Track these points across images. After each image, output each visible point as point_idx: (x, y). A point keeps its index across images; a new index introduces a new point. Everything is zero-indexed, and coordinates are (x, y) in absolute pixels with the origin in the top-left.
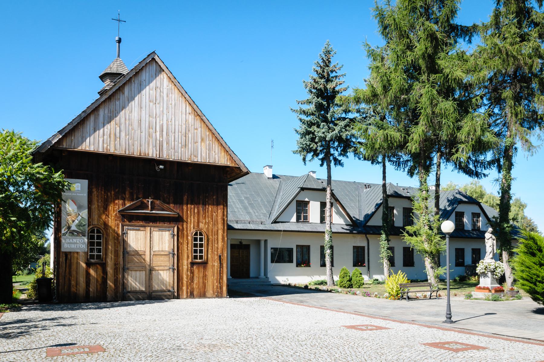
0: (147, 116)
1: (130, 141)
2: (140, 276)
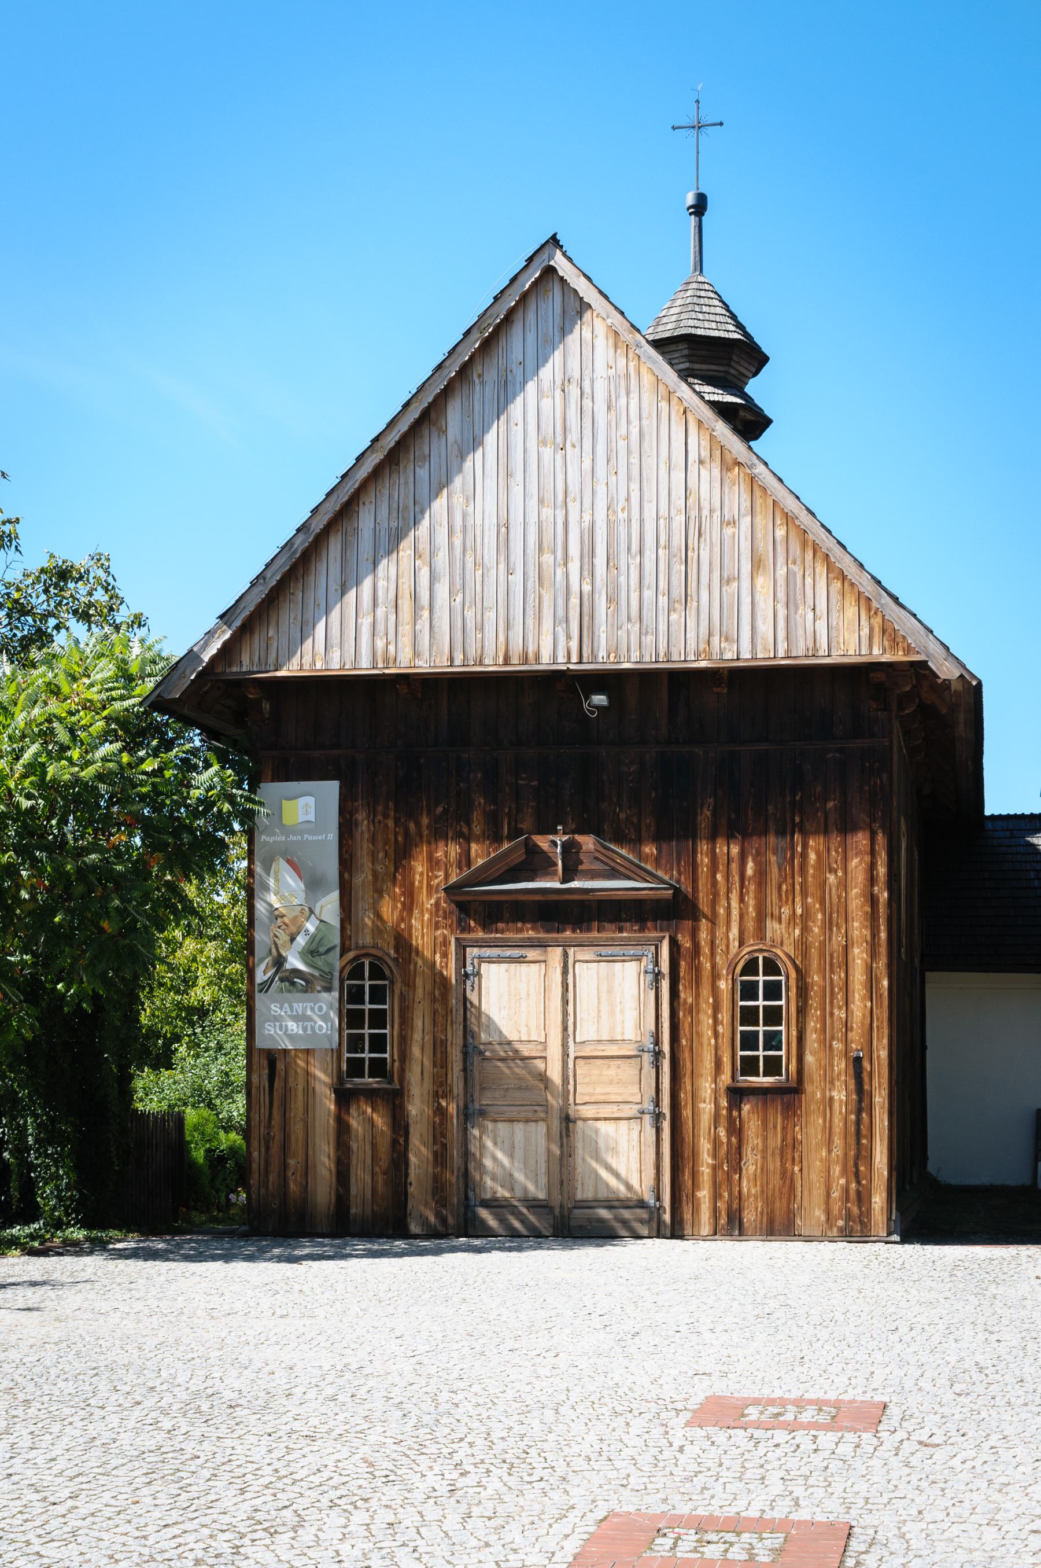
0: (533, 503)
1: (469, 614)
2: (527, 1140)
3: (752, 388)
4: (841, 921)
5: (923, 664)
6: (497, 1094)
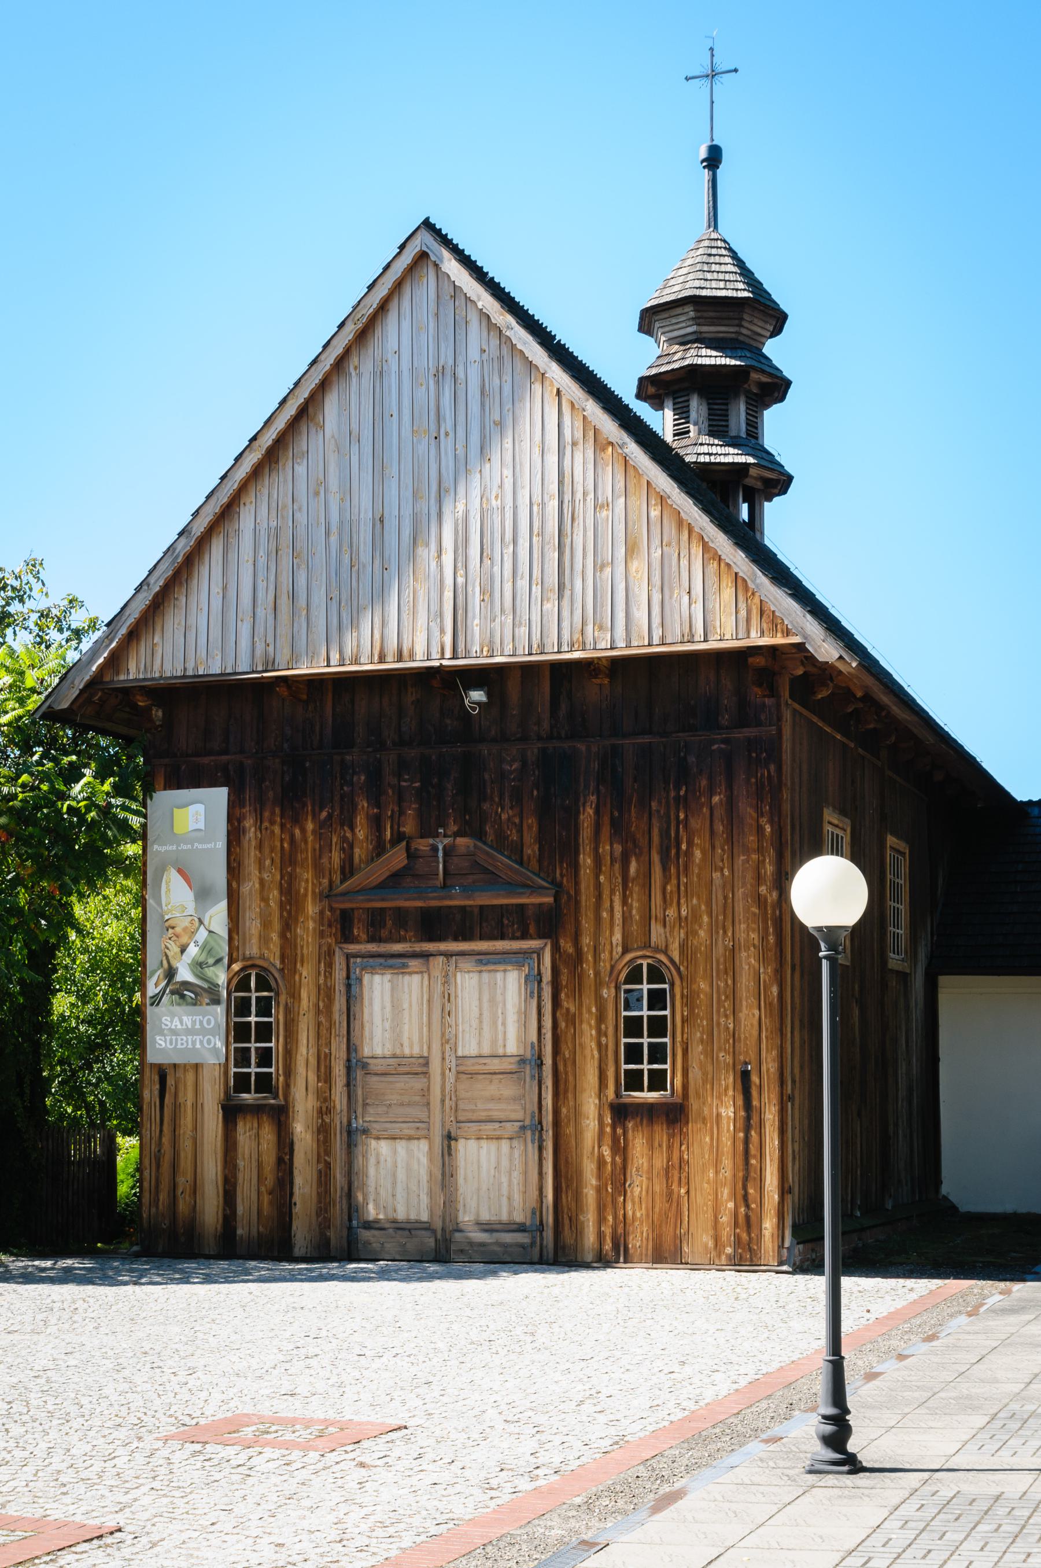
3: (771, 348)
5: (800, 647)
6: (381, 1110)
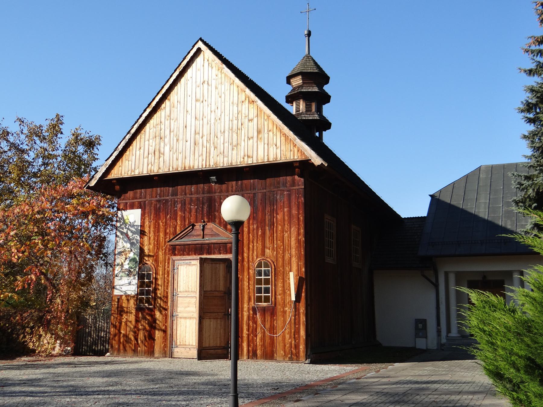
0: (193, 119)
3: (326, 88)
4: (289, 249)
